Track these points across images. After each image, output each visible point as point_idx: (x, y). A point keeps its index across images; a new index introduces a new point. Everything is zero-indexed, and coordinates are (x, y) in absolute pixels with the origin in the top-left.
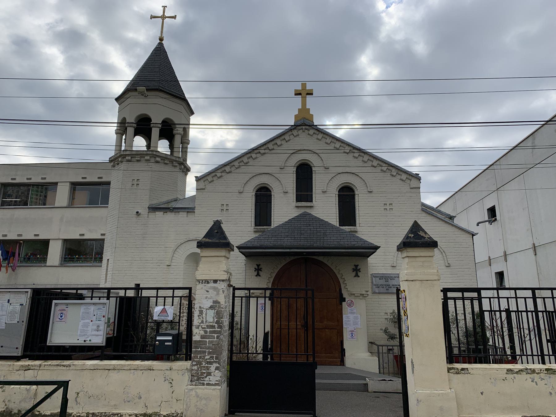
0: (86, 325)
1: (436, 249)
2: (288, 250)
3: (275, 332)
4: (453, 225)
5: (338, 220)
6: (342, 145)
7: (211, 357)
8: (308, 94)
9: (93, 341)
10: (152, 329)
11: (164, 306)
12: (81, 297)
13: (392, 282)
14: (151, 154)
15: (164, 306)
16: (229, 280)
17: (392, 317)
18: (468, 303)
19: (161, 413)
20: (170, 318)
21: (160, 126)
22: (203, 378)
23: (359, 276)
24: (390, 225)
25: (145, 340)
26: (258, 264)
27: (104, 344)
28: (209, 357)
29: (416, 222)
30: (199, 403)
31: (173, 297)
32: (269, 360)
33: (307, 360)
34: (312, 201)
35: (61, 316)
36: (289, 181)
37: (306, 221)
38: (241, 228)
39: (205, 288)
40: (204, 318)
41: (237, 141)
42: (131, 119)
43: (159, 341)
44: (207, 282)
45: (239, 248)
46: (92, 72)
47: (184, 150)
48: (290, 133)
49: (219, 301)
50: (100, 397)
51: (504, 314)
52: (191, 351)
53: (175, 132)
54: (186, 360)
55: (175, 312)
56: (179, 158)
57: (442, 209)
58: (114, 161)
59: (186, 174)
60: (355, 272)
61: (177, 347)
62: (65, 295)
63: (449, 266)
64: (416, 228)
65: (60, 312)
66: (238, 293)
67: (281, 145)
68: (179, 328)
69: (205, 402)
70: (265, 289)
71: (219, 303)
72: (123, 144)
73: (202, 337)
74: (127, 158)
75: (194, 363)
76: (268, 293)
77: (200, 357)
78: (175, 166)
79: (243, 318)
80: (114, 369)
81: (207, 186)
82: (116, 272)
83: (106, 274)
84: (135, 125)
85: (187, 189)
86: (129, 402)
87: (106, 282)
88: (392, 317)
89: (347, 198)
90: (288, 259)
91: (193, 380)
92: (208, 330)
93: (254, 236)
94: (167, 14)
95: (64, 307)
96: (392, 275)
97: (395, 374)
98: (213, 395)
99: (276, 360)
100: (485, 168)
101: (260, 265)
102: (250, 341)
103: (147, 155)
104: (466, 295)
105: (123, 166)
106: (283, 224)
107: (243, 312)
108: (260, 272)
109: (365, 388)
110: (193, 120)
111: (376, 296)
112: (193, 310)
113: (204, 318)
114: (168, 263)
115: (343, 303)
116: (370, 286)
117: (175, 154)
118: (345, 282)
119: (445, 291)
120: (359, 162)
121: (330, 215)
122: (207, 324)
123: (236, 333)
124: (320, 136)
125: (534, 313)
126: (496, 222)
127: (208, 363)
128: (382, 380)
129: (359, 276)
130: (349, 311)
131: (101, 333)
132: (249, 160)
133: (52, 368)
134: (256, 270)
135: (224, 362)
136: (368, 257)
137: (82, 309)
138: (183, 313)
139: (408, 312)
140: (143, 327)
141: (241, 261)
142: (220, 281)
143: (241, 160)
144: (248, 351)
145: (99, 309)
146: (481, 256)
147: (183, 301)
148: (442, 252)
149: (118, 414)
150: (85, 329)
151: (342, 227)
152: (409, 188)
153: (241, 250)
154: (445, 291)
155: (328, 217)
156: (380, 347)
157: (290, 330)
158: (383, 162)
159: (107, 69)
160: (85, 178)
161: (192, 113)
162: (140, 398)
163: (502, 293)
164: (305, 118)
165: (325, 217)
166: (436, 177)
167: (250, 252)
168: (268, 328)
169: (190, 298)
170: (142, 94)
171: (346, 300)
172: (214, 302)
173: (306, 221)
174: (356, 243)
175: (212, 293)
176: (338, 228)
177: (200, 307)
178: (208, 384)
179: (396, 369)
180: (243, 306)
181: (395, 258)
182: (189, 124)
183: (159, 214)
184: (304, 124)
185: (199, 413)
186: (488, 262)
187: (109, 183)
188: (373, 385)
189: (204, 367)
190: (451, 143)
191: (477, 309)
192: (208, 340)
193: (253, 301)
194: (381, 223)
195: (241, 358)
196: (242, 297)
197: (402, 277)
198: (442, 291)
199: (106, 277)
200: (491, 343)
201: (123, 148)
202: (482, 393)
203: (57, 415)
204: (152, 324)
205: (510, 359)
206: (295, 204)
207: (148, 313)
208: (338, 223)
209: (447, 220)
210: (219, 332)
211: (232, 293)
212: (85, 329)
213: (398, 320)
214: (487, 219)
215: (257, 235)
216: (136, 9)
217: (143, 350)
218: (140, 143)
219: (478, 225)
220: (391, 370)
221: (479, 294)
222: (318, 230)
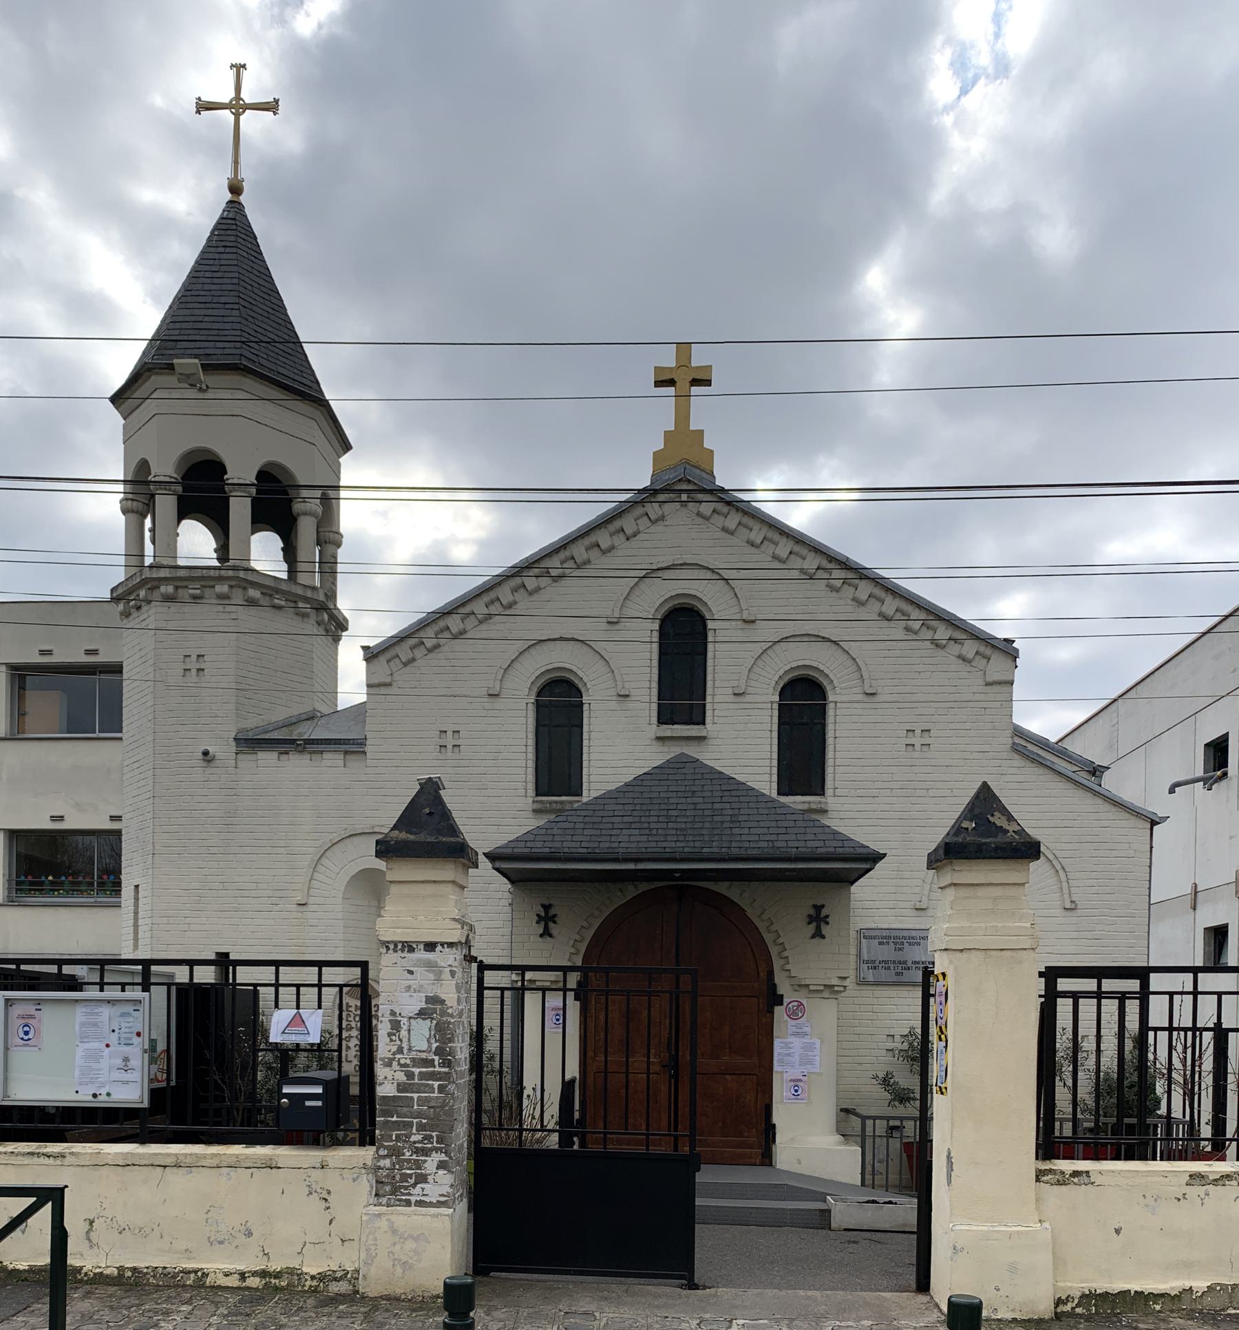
0: (94, 1057)
1: (1033, 865)
2: (631, 866)
3: (590, 1080)
4: (1096, 794)
5: (775, 778)
6: (797, 548)
7: (425, 1138)
8: (696, 382)
9: (115, 1097)
10: (270, 1068)
11: (298, 1007)
12: (73, 984)
13: (914, 954)
14: (231, 574)
15: (298, 1007)
16: (467, 944)
17: (906, 1046)
18: (1110, 1006)
19: (305, 1270)
20: (315, 1038)
21: (253, 491)
22: (406, 1188)
23: (823, 937)
24: (919, 793)
25: (252, 1096)
26: (546, 903)
27: (146, 1104)
28: (419, 1137)
29: (985, 786)
30: (398, 1247)
31: (320, 986)
32: (576, 1147)
33: (676, 1149)
34: (703, 722)
35: (26, 1033)
36: (638, 663)
37: (682, 781)
38: (497, 803)
39: (404, 963)
40: (405, 1040)
41: (484, 544)
42: (165, 468)
43: (287, 1096)
44: (409, 947)
45: (492, 857)
46: (41, 315)
47: (326, 568)
48: (639, 510)
49: (443, 996)
50: (148, 1230)
51: (1208, 1037)
52: (373, 1123)
53: (297, 507)
54: (362, 1144)
55: (328, 1027)
56: (314, 588)
57: (1076, 747)
58: (129, 597)
59: (337, 639)
60: (814, 924)
61: (338, 1111)
62: (31, 978)
63: (1072, 908)
64: (985, 801)
65: (23, 1021)
66: (491, 978)
67: (613, 548)
68: (340, 1067)
69: (414, 1245)
70: (565, 970)
71: (442, 1002)
72: (149, 548)
73: (401, 1087)
74: (163, 589)
75: (383, 1152)
76: (573, 980)
77: (397, 1136)
78: (304, 616)
79: (507, 1044)
80: (177, 1166)
81: (396, 677)
82: (164, 915)
83: (136, 926)
84: (179, 489)
85: (342, 687)
86: (221, 1243)
87: (136, 947)
88: (906, 1046)
89: (803, 709)
90: (631, 891)
91: (381, 1192)
92: (417, 1071)
93: (534, 823)
94: (247, 97)
95: (31, 1009)
96: (914, 934)
97: (902, 1189)
98: (426, 1240)
99: (595, 1148)
100: (1203, 629)
101: (550, 906)
102: (525, 1102)
103: (221, 579)
104: (1109, 985)
105: (154, 614)
106: (618, 790)
107: (507, 1030)
108: (551, 925)
109: (823, 1219)
110: (351, 471)
111: (868, 992)
112: (374, 1022)
113: (405, 1040)
114: (300, 898)
115: (777, 1009)
116: (853, 965)
117: (302, 578)
118: (785, 954)
119: (1051, 975)
120: (842, 605)
121: (752, 763)
122: (413, 1055)
123: (490, 1081)
124: (733, 520)
125: (14, 967)
126: (1224, 783)
127: (417, 1151)
128: (868, 1202)
129: (823, 937)
130: (791, 1029)
131: (136, 1076)
132: (518, 596)
133: (13, 1160)
134: (540, 919)
135: (460, 1151)
136: (852, 883)
137: (80, 1013)
138: (350, 1029)
139: (950, 1033)
140: (244, 1068)
141: (499, 895)
142: (442, 944)
143: (492, 595)
144: (521, 1125)
145: (123, 1015)
146: (1169, 881)
147: (346, 999)
148: (1059, 870)
149: (196, 1272)
150: (95, 1066)
151: (783, 799)
152: (981, 682)
153: (498, 865)
154: (1051, 975)
155: (748, 770)
156: (869, 1123)
157: (631, 1076)
158: (912, 603)
159: (87, 310)
160: (49, 653)
161: (346, 446)
162: (249, 1234)
163: (1209, 981)
164: (687, 462)
165: (738, 770)
166: (1066, 653)
167: (524, 869)
168: (573, 1071)
169: (365, 991)
170: (190, 381)
171: (786, 1001)
172: (429, 1000)
173: (682, 781)
174: (821, 844)
175: (423, 978)
176: (773, 801)
177: (393, 1013)
178: (420, 1203)
179: (906, 1175)
180: (507, 1015)
181: (927, 887)
182: (337, 488)
183: (267, 758)
184: (685, 482)
185: (399, 1270)
186: (1189, 899)
187: (117, 669)
188: (843, 1213)
189: (408, 1161)
190: (1117, 550)
191: (1133, 1024)
192: (415, 1096)
193: (532, 1002)
194: (894, 785)
195: (506, 1139)
196: (502, 990)
197: (936, 940)
198: (1041, 974)
199: (136, 932)
200: (1163, 1111)
201: (148, 561)
202: (1118, 1231)
203: (45, 1271)
204: (270, 1057)
205: (1209, 1149)
206: (654, 730)
207: (257, 1028)
208: (775, 786)
209: (1083, 777)
210: (446, 1077)
211: (475, 980)
212: (95, 1066)
213: (920, 1053)
214: (1200, 772)
215: (541, 821)
216: (158, 101)
217: (250, 1118)
218: (196, 542)
219: (1172, 791)
220: (893, 1178)
221: (1145, 984)
222: (716, 806)
